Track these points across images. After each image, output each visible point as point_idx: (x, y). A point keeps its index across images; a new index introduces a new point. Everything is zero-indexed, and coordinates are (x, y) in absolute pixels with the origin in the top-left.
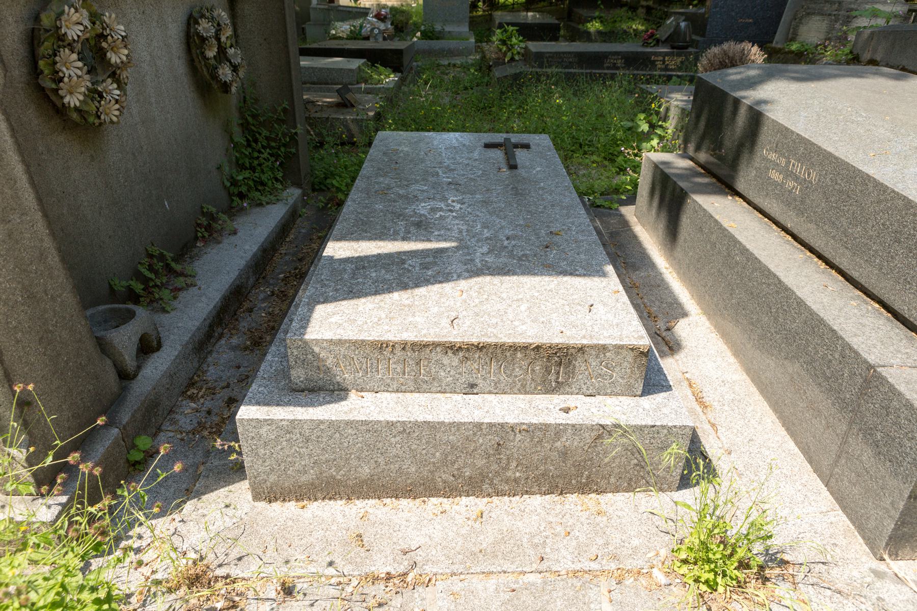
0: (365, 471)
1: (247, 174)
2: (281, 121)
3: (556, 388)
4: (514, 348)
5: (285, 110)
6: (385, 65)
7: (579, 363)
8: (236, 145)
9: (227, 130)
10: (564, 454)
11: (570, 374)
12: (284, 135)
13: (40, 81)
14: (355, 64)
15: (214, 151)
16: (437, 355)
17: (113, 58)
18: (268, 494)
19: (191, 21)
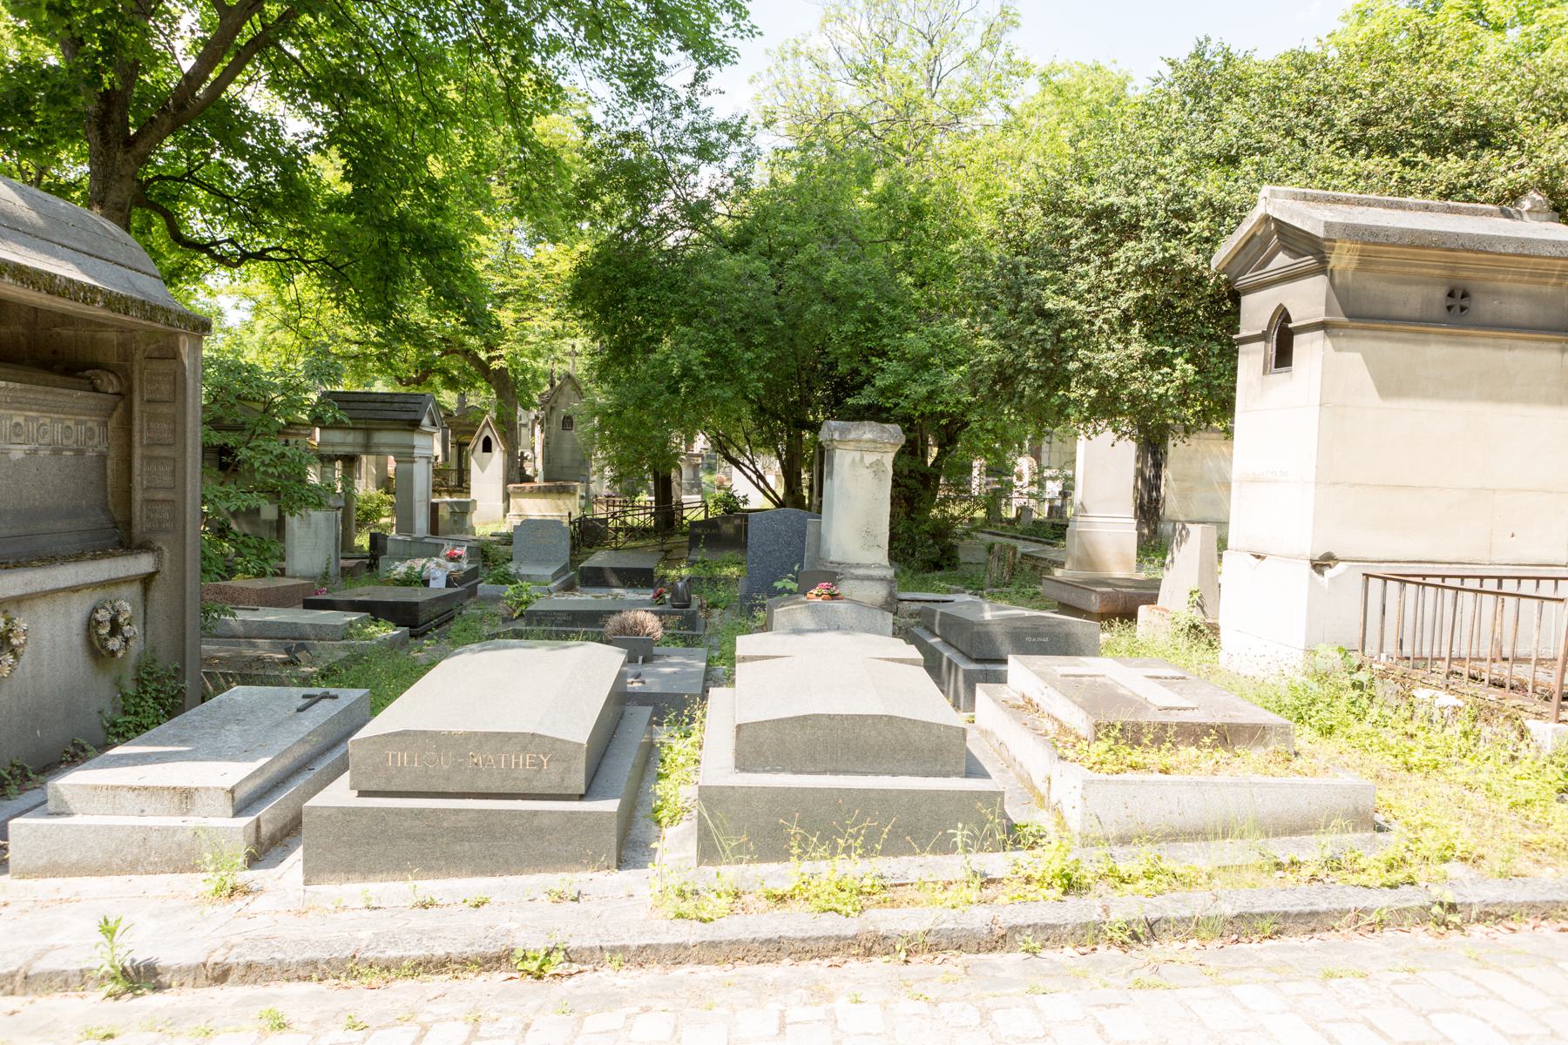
0: (74, 857)
1: (129, 718)
2: (171, 678)
3: (187, 812)
4: (163, 789)
5: (176, 670)
6: (388, 619)
7: (196, 797)
8: (124, 696)
9: (118, 683)
10: (179, 845)
11: (193, 804)
12: (173, 688)
13: (895, 429)
14: (353, 617)
15: (100, 696)
16: (124, 792)
17: (15, 641)
18: (25, 874)
19: (95, 610)
